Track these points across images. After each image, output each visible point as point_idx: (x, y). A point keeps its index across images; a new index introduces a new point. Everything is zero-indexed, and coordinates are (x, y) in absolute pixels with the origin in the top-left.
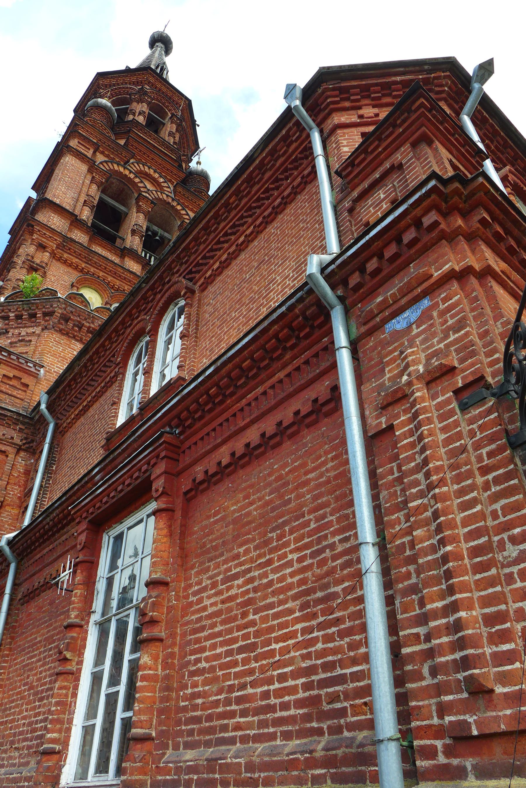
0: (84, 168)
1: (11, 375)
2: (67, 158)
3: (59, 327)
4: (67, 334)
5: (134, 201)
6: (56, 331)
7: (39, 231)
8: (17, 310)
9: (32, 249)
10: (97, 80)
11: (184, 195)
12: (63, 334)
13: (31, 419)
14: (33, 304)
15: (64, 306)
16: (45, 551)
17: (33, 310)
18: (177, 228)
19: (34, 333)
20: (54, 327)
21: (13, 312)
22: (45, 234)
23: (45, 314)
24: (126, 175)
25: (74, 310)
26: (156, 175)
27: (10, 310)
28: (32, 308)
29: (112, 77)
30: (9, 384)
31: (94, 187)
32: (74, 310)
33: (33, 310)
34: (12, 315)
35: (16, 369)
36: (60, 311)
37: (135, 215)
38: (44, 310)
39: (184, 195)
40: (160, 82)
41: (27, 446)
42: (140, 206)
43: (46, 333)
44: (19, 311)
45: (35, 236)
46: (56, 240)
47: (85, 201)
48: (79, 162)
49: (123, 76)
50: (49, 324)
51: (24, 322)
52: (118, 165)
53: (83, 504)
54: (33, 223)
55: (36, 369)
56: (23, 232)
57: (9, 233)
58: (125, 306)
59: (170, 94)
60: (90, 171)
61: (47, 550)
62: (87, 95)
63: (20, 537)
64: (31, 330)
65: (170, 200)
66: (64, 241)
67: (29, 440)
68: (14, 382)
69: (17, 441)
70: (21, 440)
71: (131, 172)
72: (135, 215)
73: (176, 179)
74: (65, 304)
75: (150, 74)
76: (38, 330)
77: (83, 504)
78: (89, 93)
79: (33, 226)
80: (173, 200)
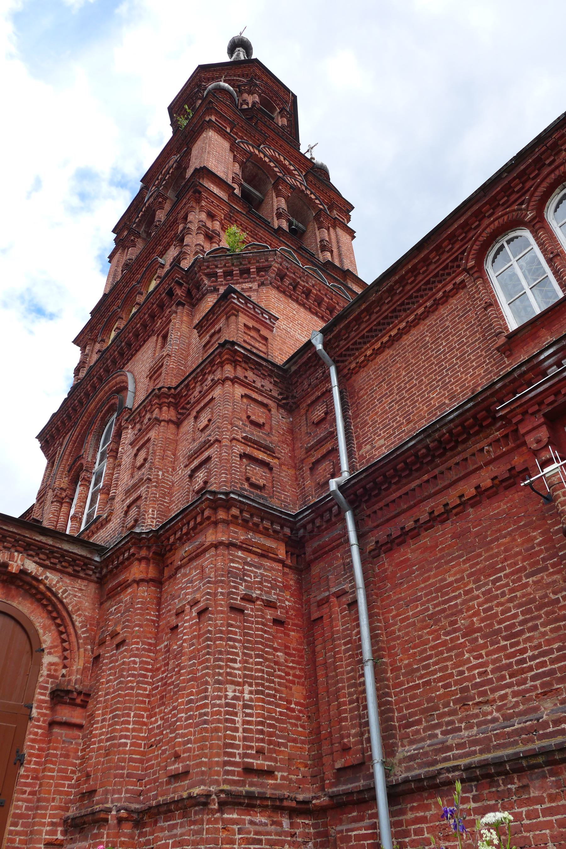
0: (227, 145)
1: (250, 325)
2: (210, 133)
3: (276, 284)
4: (284, 292)
5: (270, 187)
6: (274, 287)
7: (207, 198)
8: (225, 265)
9: (203, 216)
10: (198, 73)
11: (315, 185)
12: (280, 291)
13: (285, 371)
14: (244, 258)
15: (280, 260)
16: (413, 485)
17: (244, 265)
18: (312, 218)
19: (251, 288)
20: (271, 284)
21: (221, 268)
22: (212, 202)
23: (259, 270)
24: (261, 158)
25: (289, 266)
26: (287, 163)
27: (217, 267)
28: (243, 263)
29: (214, 70)
30: (249, 335)
31: (237, 165)
32: (289, 266)
33: (244, 265)
34: (220, 271)
35: (253, 319)
36: (276, 265)
37: (275, 199)
38: (258, 264)
39: (315, 185)
40: (267, 76)
41: (284, 401)
42: (280, 190)
43: (264, 289)
44: (229, 267)
45: (203, 203)
46: (223, 209)
47: (233, 178)
48: (222, 139)
49: (227, 69)
50: (267, 279)
51: (235, 278)
52: (253, 147)
53: (530, 395)
54: (201, 190)
55: (271, 322)
56: (189, 200)
57: (114, 231)
58: (468, 206)
59: (276, 89)
60: (232, 150)
61: (418, 482)
62: (185, 90)
63: (362, 476)
64: (246, 286)
65: (304, 188)
66: (230, 212)
67: (285, 396)
68: (253, 333)
69: (275, 394)
70: (280, 394)
71: (265, 156)
72: (275, 199)
73: (304, 169)
74: (281, 258)
75: (257, 66)
76: (255, 286)
77: (530, 395)
78: (187, 87)
79: (200, 193)
80: (306, 188)
